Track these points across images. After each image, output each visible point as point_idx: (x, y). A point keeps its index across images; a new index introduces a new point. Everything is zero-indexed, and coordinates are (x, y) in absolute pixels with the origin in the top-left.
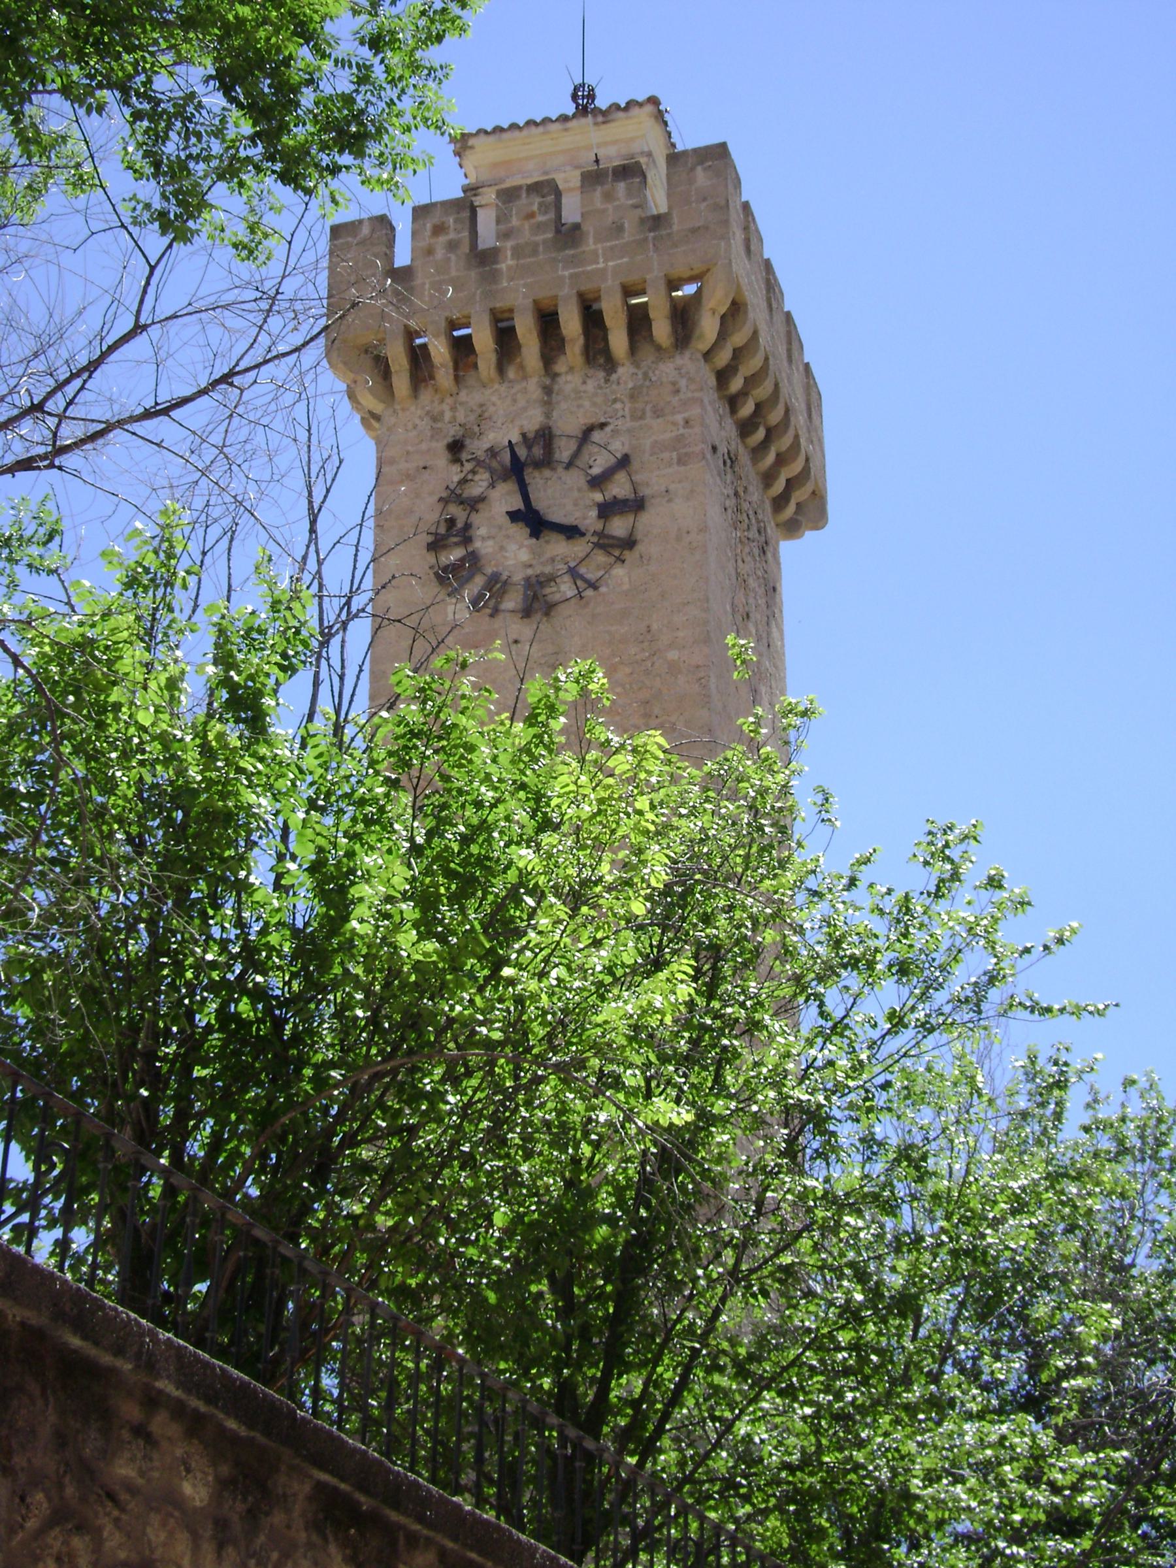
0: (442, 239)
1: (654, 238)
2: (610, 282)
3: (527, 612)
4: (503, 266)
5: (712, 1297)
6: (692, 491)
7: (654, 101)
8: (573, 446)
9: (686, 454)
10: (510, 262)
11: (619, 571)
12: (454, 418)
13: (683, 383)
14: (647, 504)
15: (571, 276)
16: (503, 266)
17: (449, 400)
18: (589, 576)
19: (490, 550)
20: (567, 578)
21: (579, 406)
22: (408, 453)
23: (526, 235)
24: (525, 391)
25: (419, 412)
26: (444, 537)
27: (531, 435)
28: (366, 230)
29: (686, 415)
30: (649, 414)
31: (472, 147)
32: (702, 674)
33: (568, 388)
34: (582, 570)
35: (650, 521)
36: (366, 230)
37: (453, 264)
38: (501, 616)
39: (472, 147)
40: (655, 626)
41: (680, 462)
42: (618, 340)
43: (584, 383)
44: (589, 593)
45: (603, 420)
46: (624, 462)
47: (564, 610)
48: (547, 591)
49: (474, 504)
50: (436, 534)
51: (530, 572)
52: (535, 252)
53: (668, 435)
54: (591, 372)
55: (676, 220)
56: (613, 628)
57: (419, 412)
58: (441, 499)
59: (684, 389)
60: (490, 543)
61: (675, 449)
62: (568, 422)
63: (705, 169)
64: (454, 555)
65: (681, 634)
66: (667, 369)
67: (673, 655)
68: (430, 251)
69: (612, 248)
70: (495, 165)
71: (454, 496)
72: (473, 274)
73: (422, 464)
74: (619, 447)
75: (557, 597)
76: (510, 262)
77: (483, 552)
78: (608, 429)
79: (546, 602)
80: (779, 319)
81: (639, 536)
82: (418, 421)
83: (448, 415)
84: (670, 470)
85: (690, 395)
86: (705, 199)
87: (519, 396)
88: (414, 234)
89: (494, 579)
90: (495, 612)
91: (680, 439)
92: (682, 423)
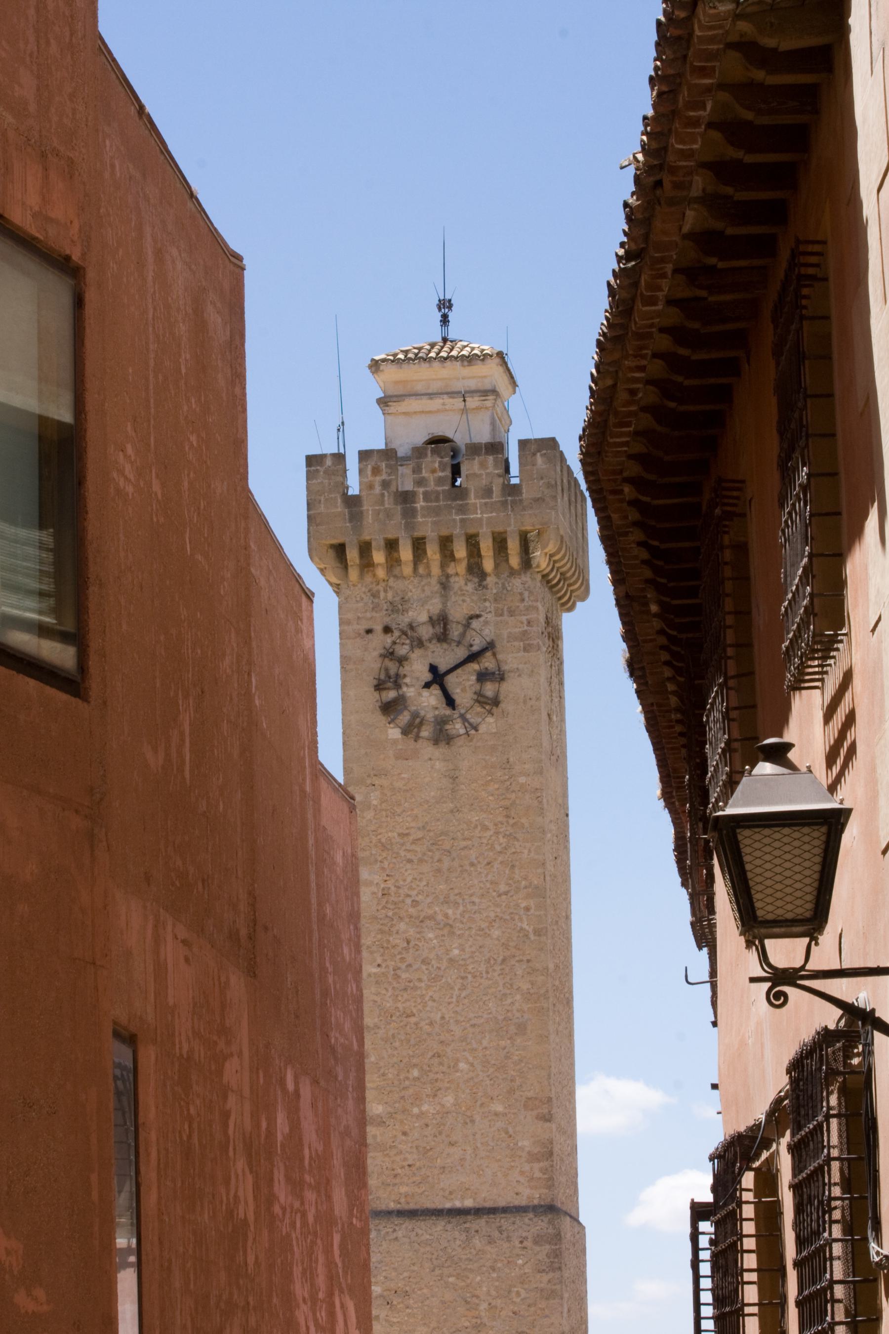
0: (378, 479)
1: (512, 501)
2: (485, 529)
3: (436, 741)
4: (418, 506)
5: (188, 475)
6: (532, 671)
7: (500, 355)
8: (460, 629)
9: (529, 645)
10: (422, 504)
11: (490, 720)
12: (386, 598)
13: (526, 594)
14: (506, 676)
15: (462, 520)
16: (418, 506)
17: (383, 584)
18: (472, 721)
19: (412, 694)
20: (459, 720)
21: (464, 601)
22: (359, 618)
23: (432, 486)
24: (429, 584)
25: (364, 589)
26: (384, 682)
27: (435, 618)
28: (329, 462)
29: (528, 617)
30: (506, 613)
31: (382, 371)
32: (539, 794)
33: (456, 586)
34: (468, 716)
35: (509, 688)
36: (329, 462)
37: (386, 498)
38: (420, 741)
39: (382, 371)
40: (511, 759)
41: (526, 649)
42: (488, 565)
43: (466, 584)
44: (473, 732)
45: (478, 613)
46: (490, 646)
47: (459, 742)
48: (448, 727)
49: (402, 661)
50: (379, 680)
51: (437, 713)
52: (437, 499)
53: (517, 630)
54: (470, 577)
55: (524, 491)
56: (488, 757)
57: (364, 589)
58: (381, 655)
59: (527, 599)
60: (412, 689)
61: (522, 640)
62: (458, 612)
63: (541, 455)
64: (392, 694)
65: (526, 766)
66: (517, 583)
67: (522, 780)
68: (371, 487)
69: (486, 504)
70: (396, 383)
71: (389, 654)
72: (399, 508)
73: (367, 627)
74: (489, 633)
75: (454, 732)
76: (422, 504)
77: (408, 695)
78: (481, 619)
79: (448, 735)
80: (565, 469)
81: (501, 697)
82: (363, 596)
83: (382, 595)
84: (519, 654)
85: (530, 603)
86: (542, 478)
87: (426, 588)
88: (361, 471)
89: (415, 715)
90: (417, 738)
91: (525, 633)
92: (525, 622)
